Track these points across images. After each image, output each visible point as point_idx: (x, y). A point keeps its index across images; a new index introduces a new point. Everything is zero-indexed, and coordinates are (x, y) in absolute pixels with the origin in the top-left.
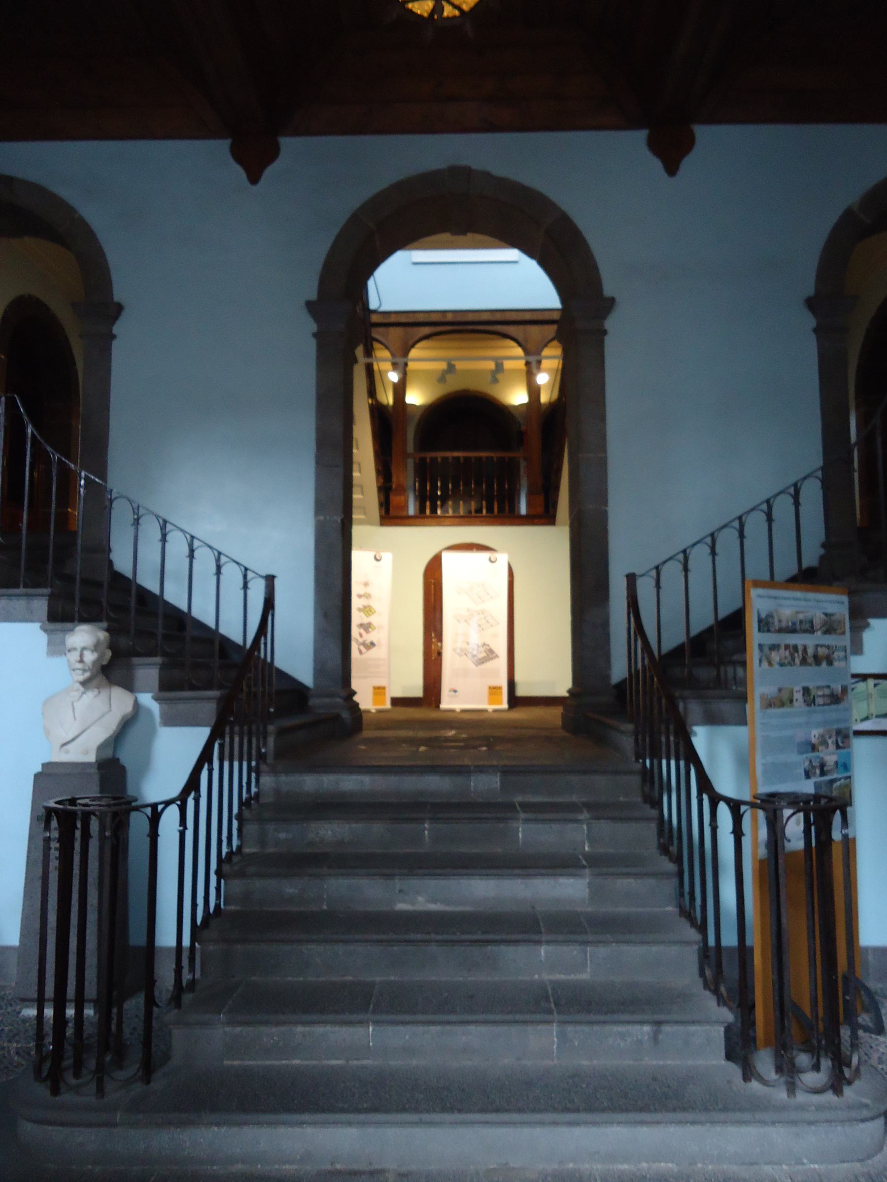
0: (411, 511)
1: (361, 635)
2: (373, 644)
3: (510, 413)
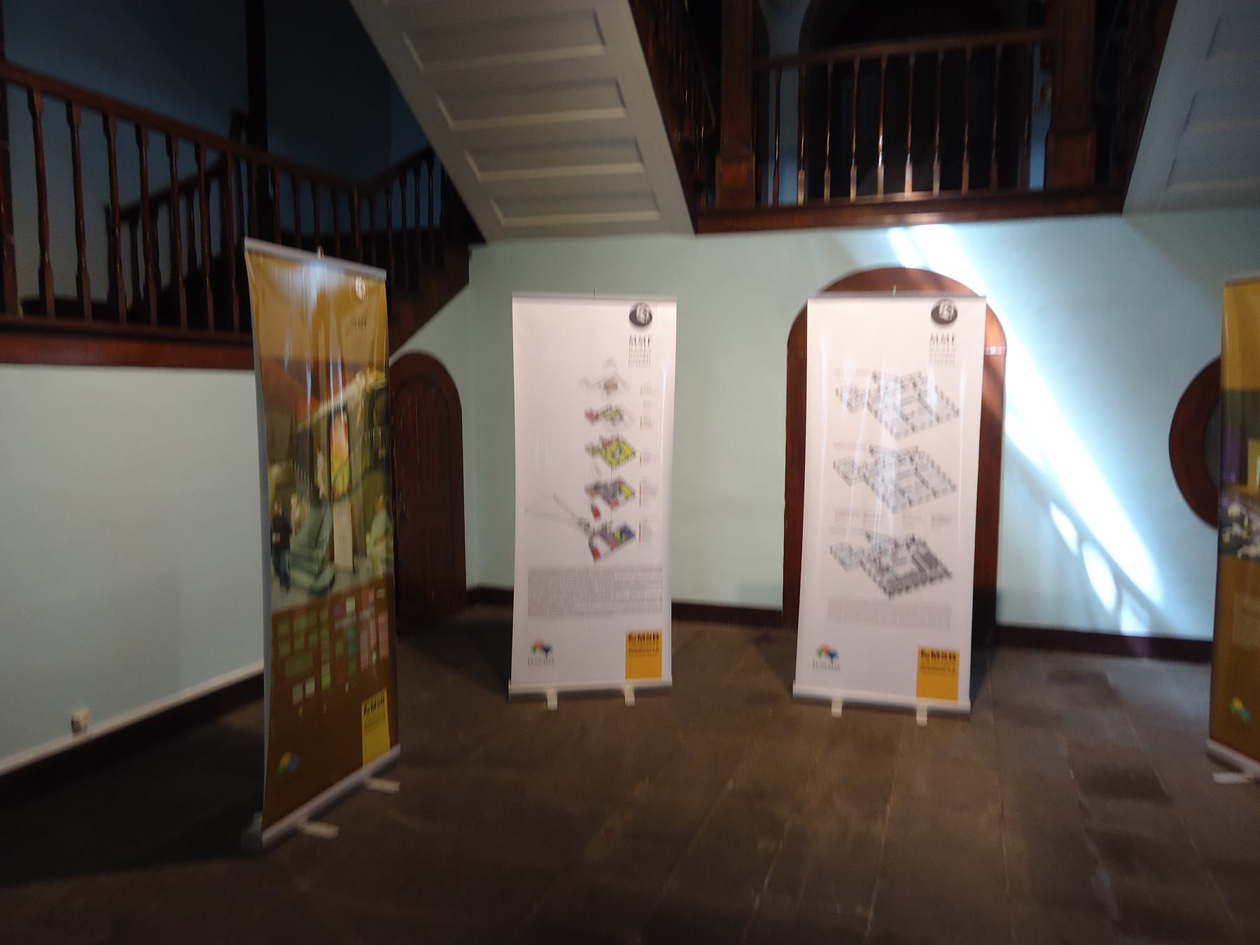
1: (596, 513)
2: (626, 533)
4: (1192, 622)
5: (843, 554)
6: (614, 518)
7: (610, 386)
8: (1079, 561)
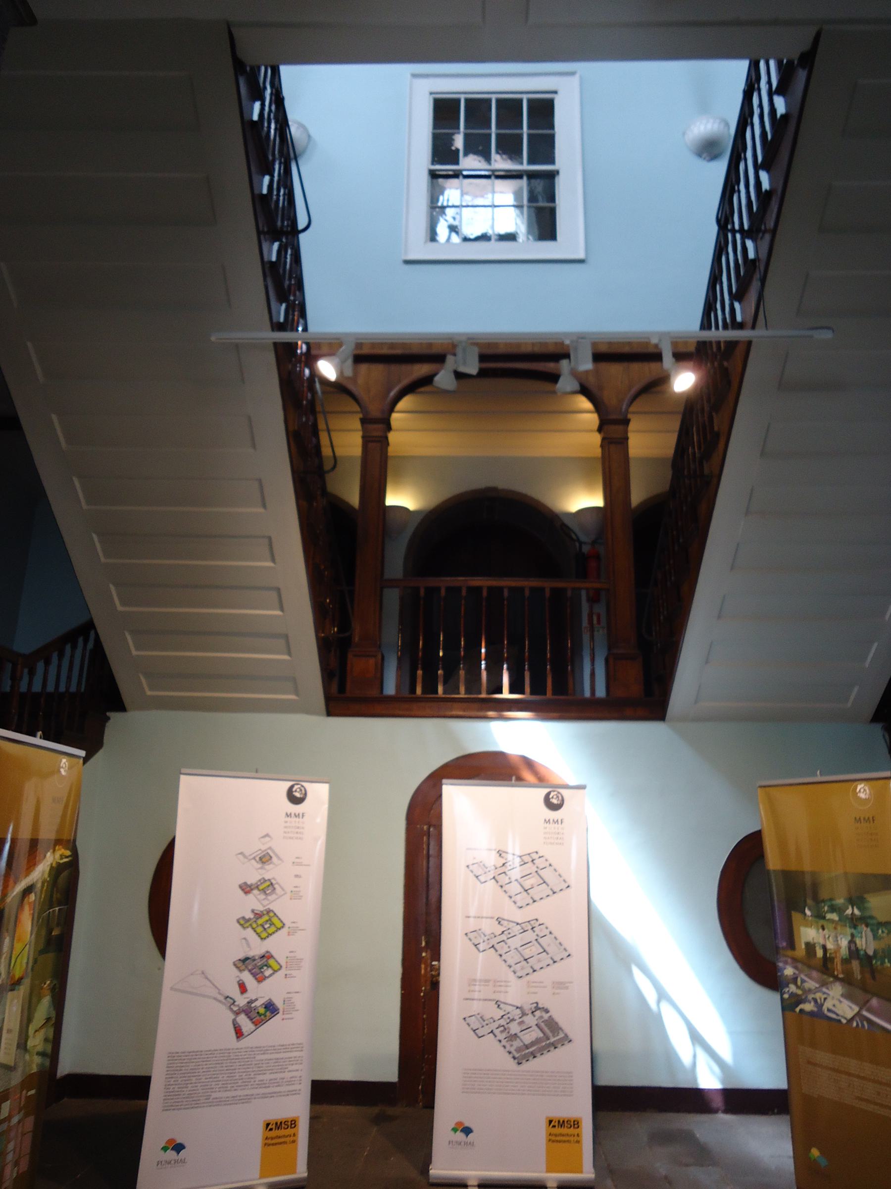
0: (390, 689)
1: (243, 988)
2: (271, 1009)
3: (564, 526)
4: (766, 1073)
5: (475, 1024)
6: (259, 993)
7: (265, 859)
8: (658, 1018)
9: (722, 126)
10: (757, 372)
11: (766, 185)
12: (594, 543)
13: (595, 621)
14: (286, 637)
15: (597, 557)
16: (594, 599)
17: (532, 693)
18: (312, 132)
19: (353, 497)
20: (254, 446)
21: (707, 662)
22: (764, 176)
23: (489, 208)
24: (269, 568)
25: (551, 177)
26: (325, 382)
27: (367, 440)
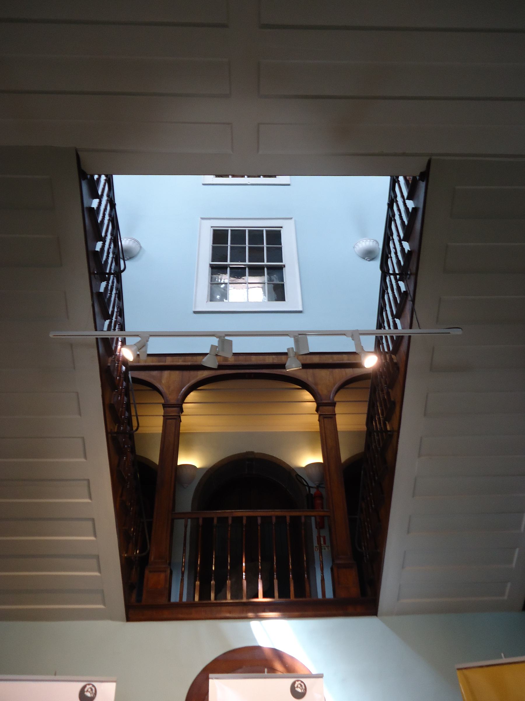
0: (175, 598)
9: (375, 242)
10: (416, 360)
11: (403, 289)
12: (318, 487)
13: (322, 542)
14: (97, 557)
15: (321, 497)
16: (320, 526)
17: (280, 597)
18: (142, 245)
19: (155, 457)
20: (80, 414)
21: (403, 567)
22: (401, 284)
23: (248, 293)
24: (88, 503)
25: (280, 269)
26: (125, 362)
27: (166, 418)
